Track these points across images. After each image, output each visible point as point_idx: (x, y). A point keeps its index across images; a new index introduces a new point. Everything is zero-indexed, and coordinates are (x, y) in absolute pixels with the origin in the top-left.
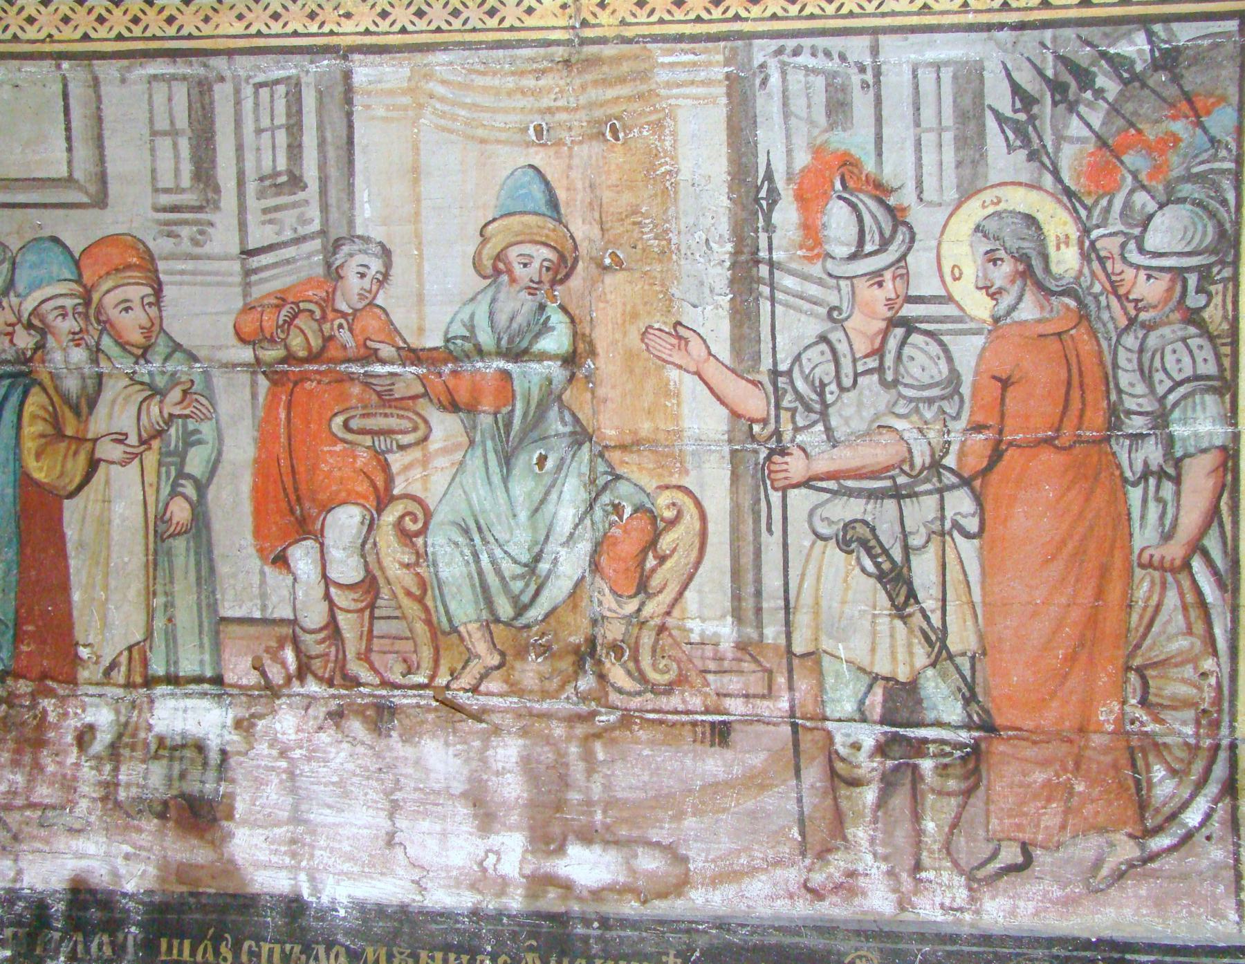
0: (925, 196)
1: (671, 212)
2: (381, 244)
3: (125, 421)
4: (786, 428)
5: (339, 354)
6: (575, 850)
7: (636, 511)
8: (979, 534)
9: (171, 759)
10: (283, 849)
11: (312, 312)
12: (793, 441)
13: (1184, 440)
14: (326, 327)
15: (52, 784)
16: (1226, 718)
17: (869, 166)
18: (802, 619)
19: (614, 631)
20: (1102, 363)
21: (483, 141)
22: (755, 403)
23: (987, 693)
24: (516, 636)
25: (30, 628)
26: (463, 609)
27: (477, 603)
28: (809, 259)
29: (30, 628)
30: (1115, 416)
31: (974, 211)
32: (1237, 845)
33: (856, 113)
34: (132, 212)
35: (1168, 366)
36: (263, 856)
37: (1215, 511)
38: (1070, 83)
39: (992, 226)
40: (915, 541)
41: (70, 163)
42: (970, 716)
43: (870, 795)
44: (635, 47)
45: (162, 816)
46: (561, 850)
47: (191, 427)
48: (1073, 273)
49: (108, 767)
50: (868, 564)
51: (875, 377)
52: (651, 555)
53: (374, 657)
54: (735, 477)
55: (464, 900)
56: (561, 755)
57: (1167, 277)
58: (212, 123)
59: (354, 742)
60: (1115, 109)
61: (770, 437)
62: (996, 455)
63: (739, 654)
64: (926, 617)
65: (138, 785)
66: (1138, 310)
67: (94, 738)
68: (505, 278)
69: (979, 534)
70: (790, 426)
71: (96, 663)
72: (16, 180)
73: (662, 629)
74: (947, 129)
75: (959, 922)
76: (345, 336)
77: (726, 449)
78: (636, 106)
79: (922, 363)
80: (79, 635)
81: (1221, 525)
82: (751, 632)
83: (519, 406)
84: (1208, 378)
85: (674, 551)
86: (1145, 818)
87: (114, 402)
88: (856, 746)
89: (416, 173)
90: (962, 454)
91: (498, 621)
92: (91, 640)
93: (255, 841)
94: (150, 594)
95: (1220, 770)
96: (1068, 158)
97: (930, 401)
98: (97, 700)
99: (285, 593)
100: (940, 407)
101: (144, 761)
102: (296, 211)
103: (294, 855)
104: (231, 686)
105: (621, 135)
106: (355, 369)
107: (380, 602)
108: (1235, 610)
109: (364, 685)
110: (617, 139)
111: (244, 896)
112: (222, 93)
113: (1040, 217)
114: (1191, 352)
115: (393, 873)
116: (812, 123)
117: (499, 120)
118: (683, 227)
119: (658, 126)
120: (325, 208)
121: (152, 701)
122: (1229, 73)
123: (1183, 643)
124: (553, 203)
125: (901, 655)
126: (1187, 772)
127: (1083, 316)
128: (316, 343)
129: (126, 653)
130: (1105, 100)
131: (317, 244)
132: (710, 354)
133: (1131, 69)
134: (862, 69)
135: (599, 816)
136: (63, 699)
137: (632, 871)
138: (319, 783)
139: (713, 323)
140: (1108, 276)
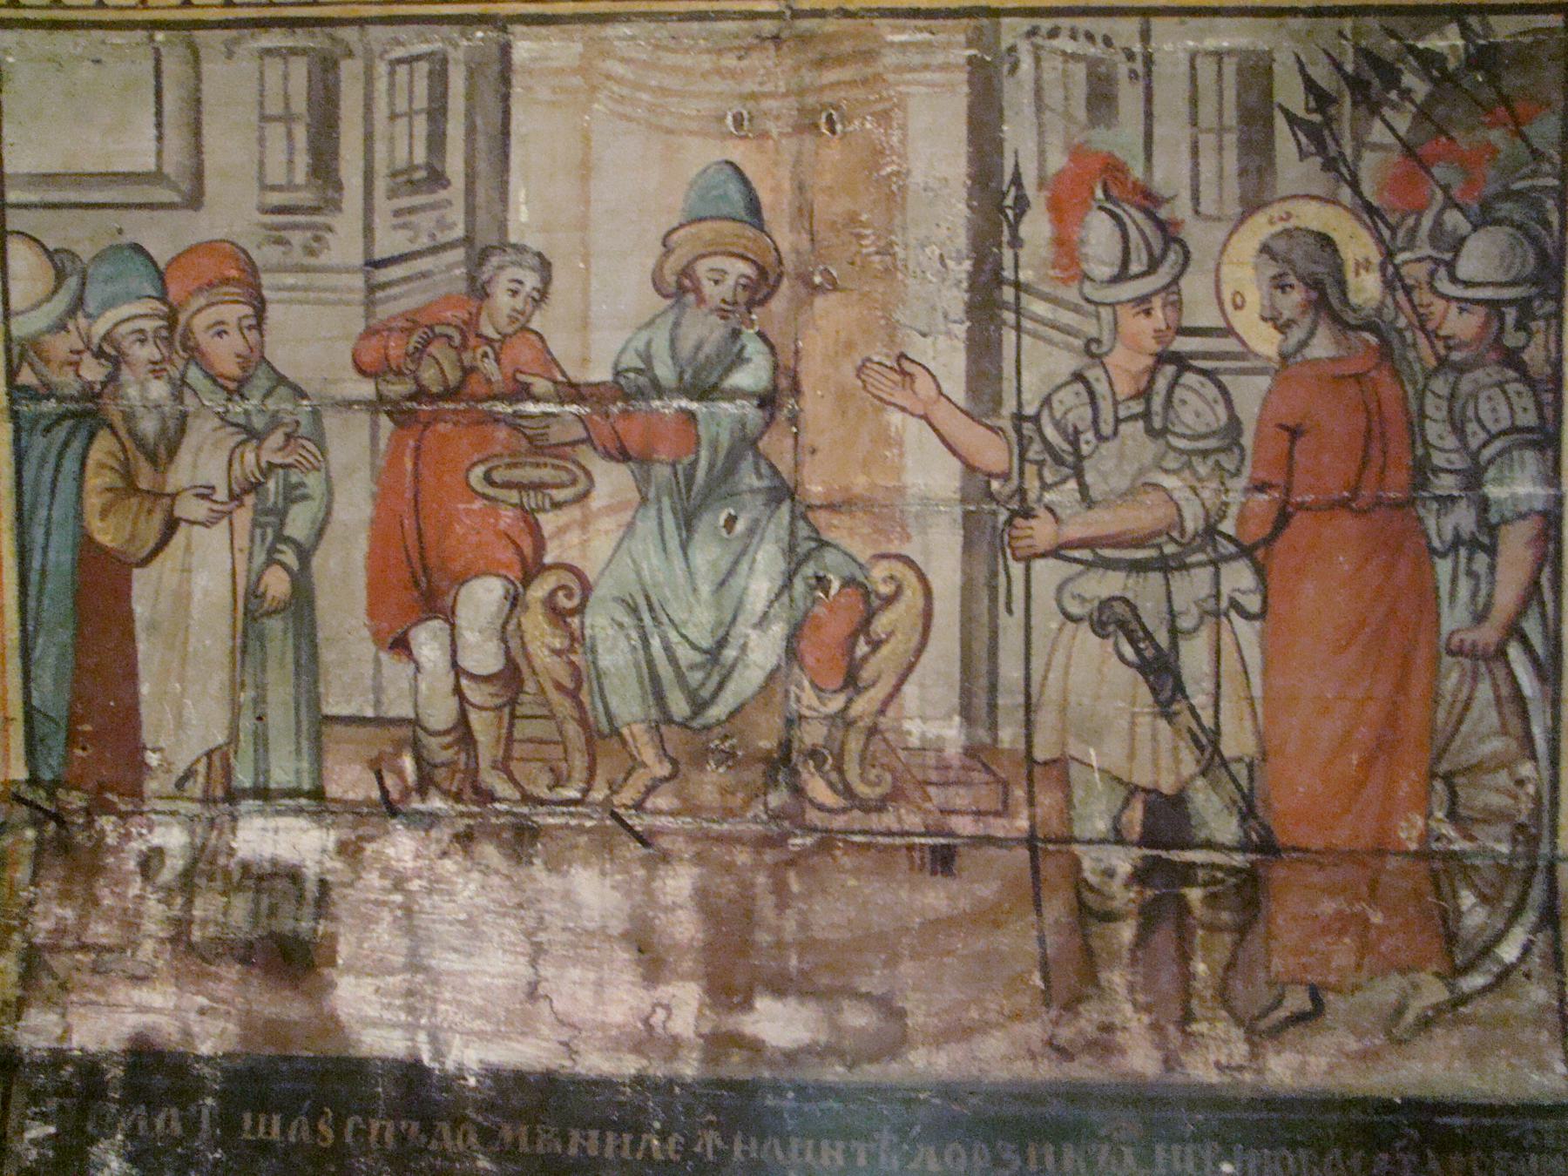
0: (1202, 209)
1: (898, 221)
2: (539, 255)
3: (213, 471)
4: (1033, 485)
5: (481, 390)
6: (763, 1003)
7: (843, 586)
8: (1262, 615)
9: (258, 891)
10: (398, 1002)
11: (450, 338)
12: (1039, 500)
13: (1499, 502)
14: (467, 358)
15: (108, 921)
16: (1546, 833)
17: (1137, 172)
18: (1046, 719)
19: (813, 734)
20: (1407, 412)
21: (670, 132)
22: (993, 453)
23: (1268, 806)
24: (693, 738)
25: (87, 728)
26: (627, 705)
27: (644, 700)
28: (1064, 281)
29: (87, 728)
30: (1422, 472)
31: (1261, 228)
32: (1562, 984)
33: (1122, 110)
34: (231, 214)
35: (1482, 415)
36: (372, 1012)
37: (1535, 584)
38: (1371, 82)
39: (1280, 246)
40: (1184, 623)
41: (159, 154)
42: (1247, 835)
43: (1126, 932)
44: (859, 23)
45: (245, 960)
46: (747, 1005)
47: (294, 479)
48: (1374, 304)
49: (179, 901)
50: (1128, 651)
51: (1140, 424)
52: (862, 639)
53: (514, 765)
54: (968, 546)
55: (629, 1065)
56: (747, 888)
57: (1481, 311)
58: (337, 106)
59: (486, 871)
60: (1423, 114)
61: (1011, 497)
62: (1283, 519)
63: (968, 762)
64: (1196, 717)
65: (216, 923)
66: (1449, 348)
67: (162, 863)
68: (691, 297)
69: (1262, 615)
70: (1037, 484)
71: (168, 771)
72: (91, 175)
73: (873, 731)
74: (1229, 130)
75: (1238, 1084)
76: (489, 366)
77: (958, 511)
78: (859, 93)
79: (1196, 408)
80: (147, 736)
81: (1542, 604)
82: (983, 735)
83: (704, 454)
84: (1530, 430)
85: (890, 634)
86: (1456, 953)
87: (200, 449)
88: (1110, 873)
89: (585, 170)
90: (1241, 520)
91: (669, 720)
92: (162, 744)
93: (362, 992)
94: (236, 686)
95: (1537, 894)
96: (1371, 168)
97: (1205, 454)
98: (168, 819)
99: (405, 685)
100: (1218, 463)
101: (224, 893)
102: (435, 214)
103: (411, 1010)
104: (335, 800)
105: (839, 127)
106: (502, 408)
107: (523, 698)
108: (1556, 703)
109: (499, 800)
110: (833, 132)
111: (349, 1060)
112: (350, 71)
113: (1335, 236)
114: (1508, 398)
115: (535, 1033)
116: (1068, 117)
117: (691, 107)
118: (913, 242)
119: (884, 117)
120: (470, 211)
121: (234, 819)
122: (1551, 74)
123: (1496, 745)
124: (754, 207)
125: (1166, 761)
126: (1500, 897)
127: (1385, 351)
128: (453, 376)
129: (204, 760)
130: (1412, 101)
131: (458, 254)
132: (941, 393)
133: (1443, 70)
134: (1131, 56)
135: (794, 961)
136: (124, 816)
137: (835, 1027)
138: (443, 921)
139: (945, 357)
140: (1414, 307)
